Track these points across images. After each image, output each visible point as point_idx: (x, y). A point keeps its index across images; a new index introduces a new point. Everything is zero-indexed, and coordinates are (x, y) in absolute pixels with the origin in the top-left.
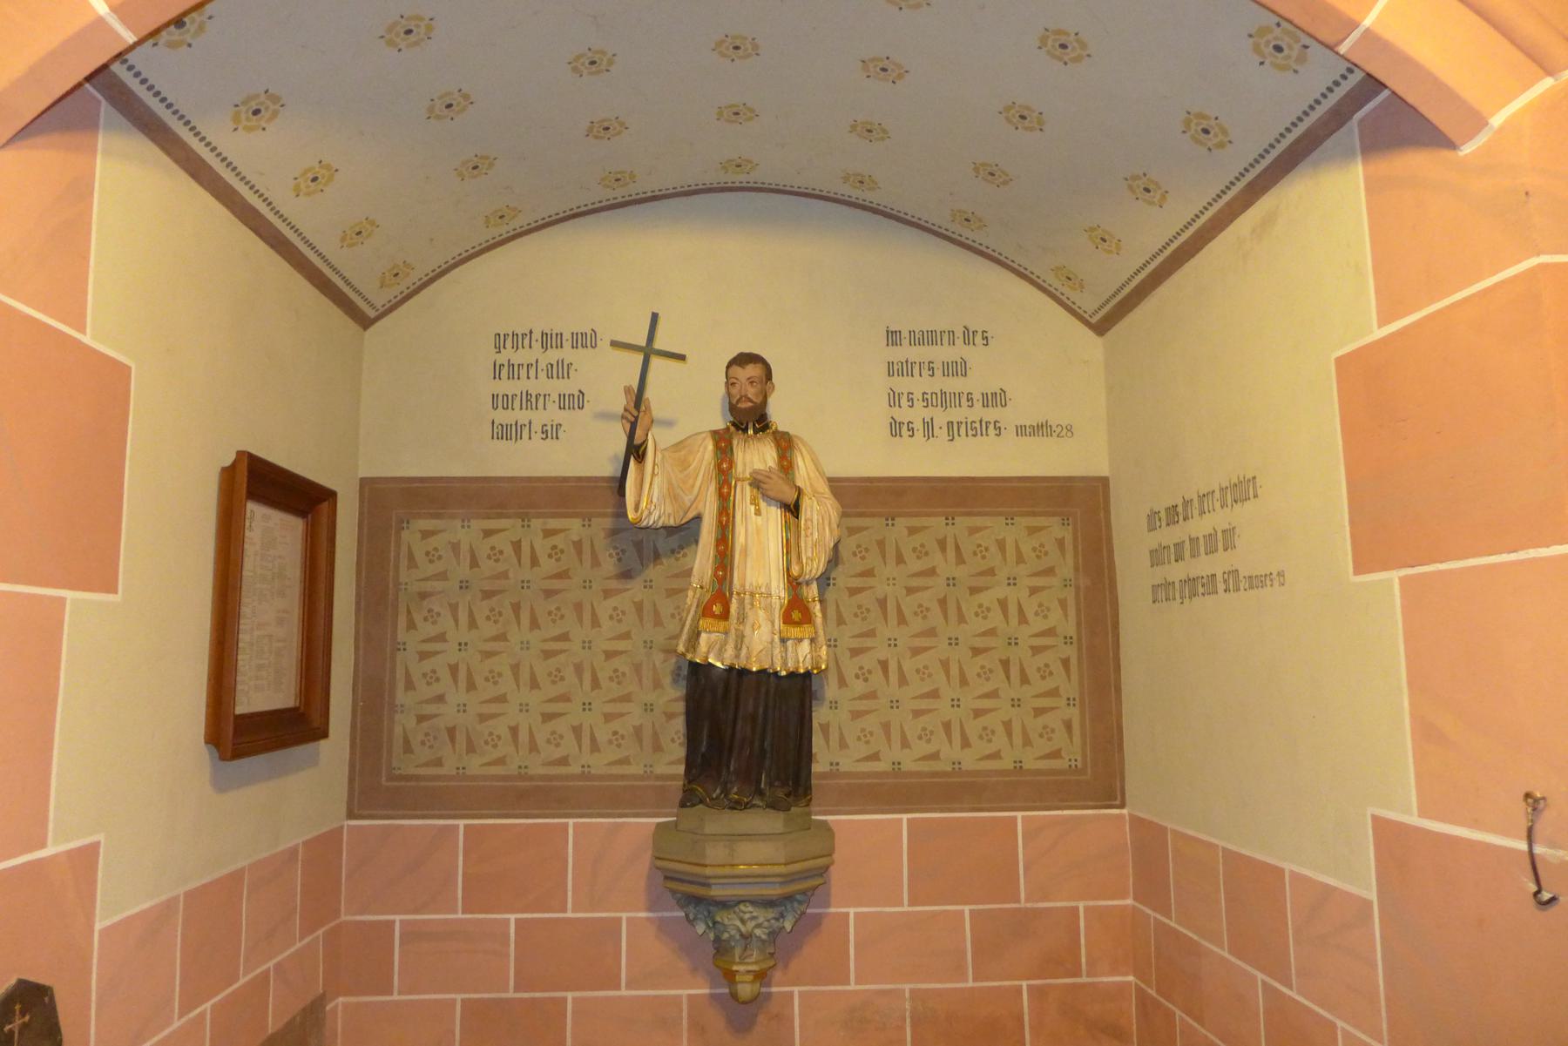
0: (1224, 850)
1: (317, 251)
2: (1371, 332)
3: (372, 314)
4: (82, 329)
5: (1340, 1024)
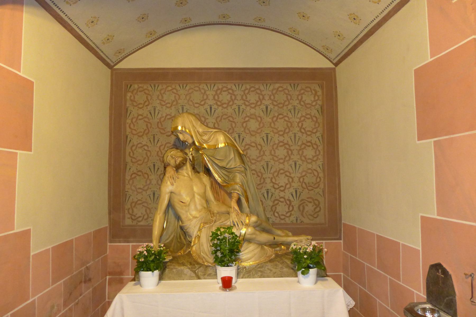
0: (377, 235)
1: (93, 42)
2: (428, 60)
3: (112, 64)
4: (20, 72)
5: (366, 264)
